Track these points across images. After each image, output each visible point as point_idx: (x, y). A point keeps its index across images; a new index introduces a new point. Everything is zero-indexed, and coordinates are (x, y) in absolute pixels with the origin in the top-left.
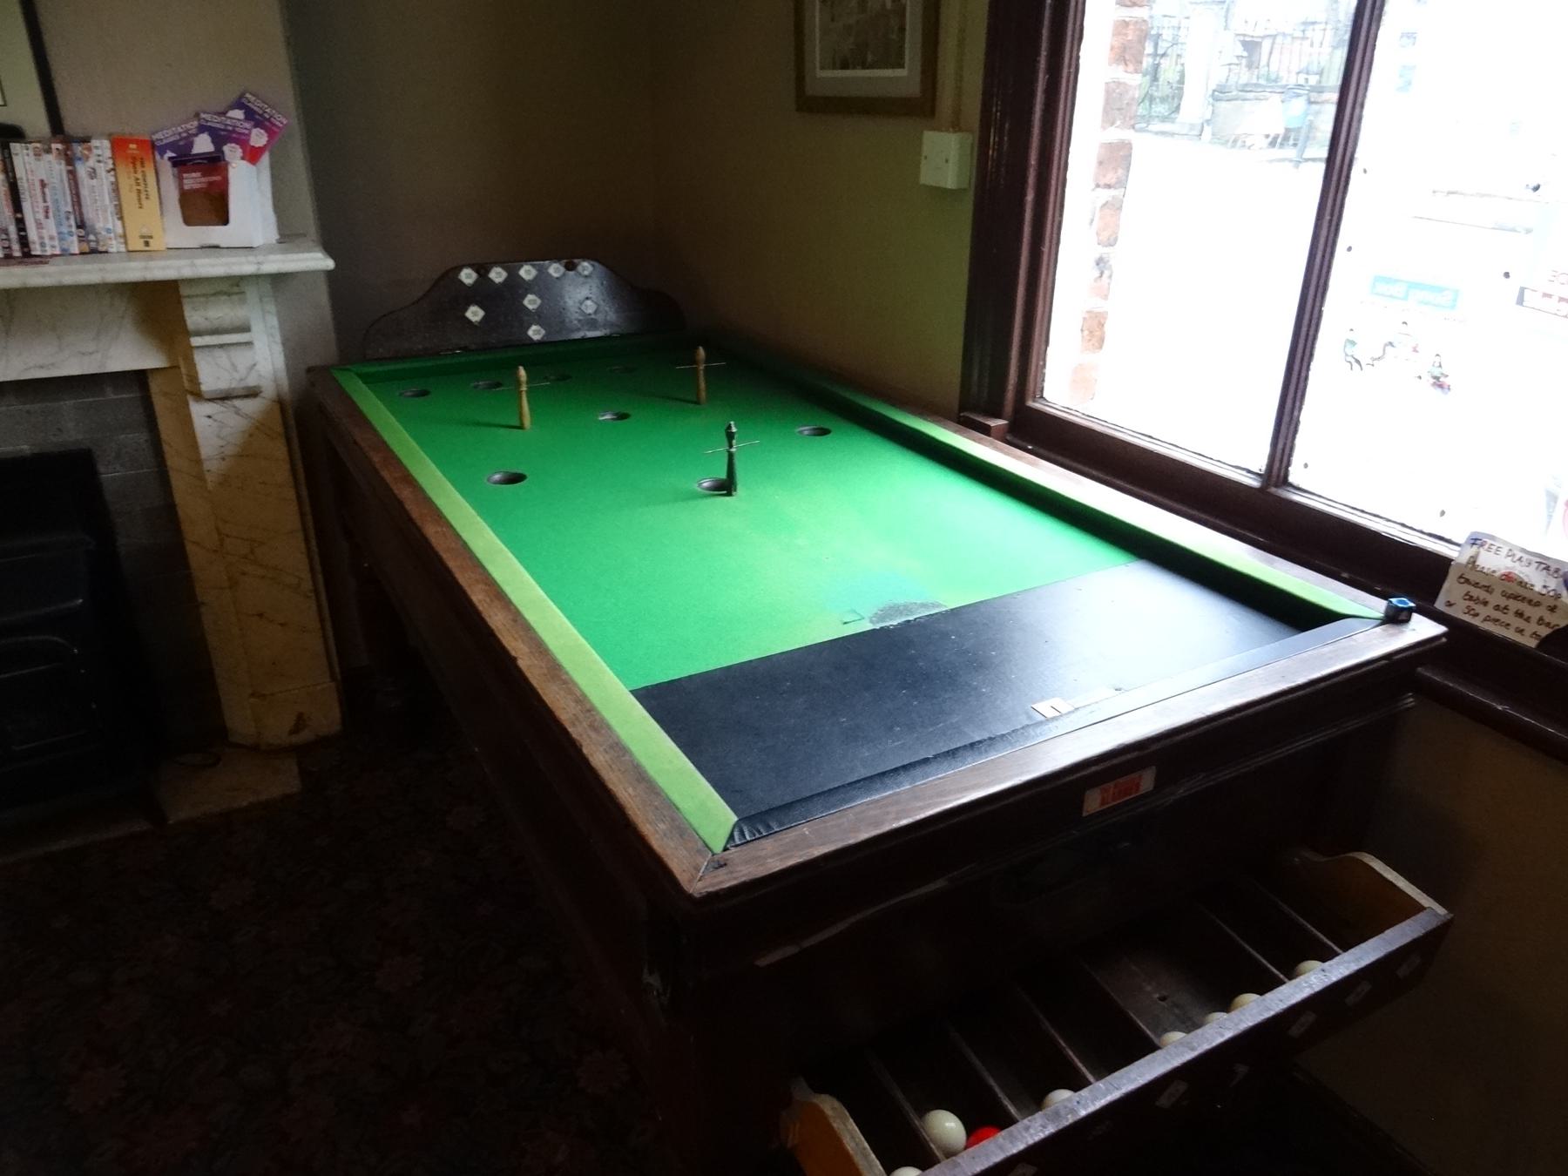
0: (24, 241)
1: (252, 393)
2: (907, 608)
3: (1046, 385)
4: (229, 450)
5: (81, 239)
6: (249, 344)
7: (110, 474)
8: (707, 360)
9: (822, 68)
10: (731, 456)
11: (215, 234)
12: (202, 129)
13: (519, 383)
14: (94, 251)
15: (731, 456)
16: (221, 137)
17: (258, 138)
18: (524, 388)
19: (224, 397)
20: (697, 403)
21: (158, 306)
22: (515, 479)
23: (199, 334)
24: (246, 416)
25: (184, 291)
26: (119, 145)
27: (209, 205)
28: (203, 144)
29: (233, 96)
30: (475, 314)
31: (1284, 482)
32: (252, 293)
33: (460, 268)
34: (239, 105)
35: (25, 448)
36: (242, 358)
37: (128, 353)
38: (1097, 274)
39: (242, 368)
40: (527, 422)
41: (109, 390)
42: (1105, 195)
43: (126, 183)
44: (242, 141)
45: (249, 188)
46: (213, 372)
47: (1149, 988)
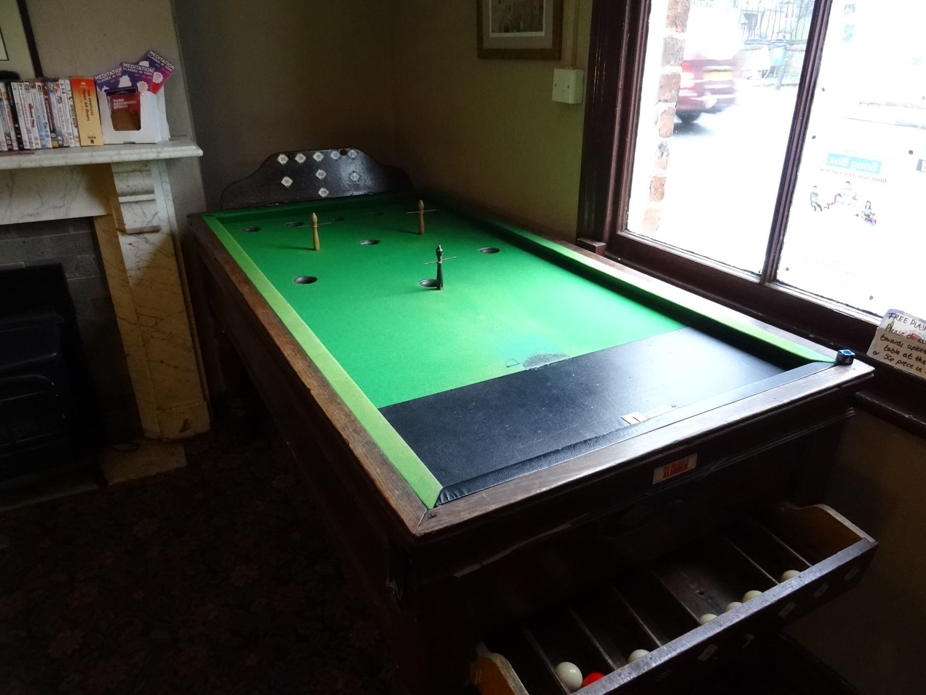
0: (20, 141)
1: (155, 230)
2: (544, 358)
3: (629, 221)
4: (143, 264)
6: (153, 200)
7: (72, 278)
8: (425, 209)
10: (439, 266)
11: (133, 135)
12: (124, 73)
13: (313, 224)
14: (61, 146)
15: (439, 266)
17: (158, 78)
19: (139, 233)
20: (420, 233)
22: (310, 280)
23: (124, 195)
25: (114, 169)
27: (129, 118)
28: (125, 82)
29: (142, 53)
31: (774, 279)
32: (155, 171)
33: (278, 155)
34: (146, 58)
35: (23, 264)
36: (149, 209)
37: (81, 206)
38: (659, 154)
39: (149, 217)
43: (79, 105)
44: (148, 80)
45: (152, 108)
46: (132, 218)
47: (693, 587)
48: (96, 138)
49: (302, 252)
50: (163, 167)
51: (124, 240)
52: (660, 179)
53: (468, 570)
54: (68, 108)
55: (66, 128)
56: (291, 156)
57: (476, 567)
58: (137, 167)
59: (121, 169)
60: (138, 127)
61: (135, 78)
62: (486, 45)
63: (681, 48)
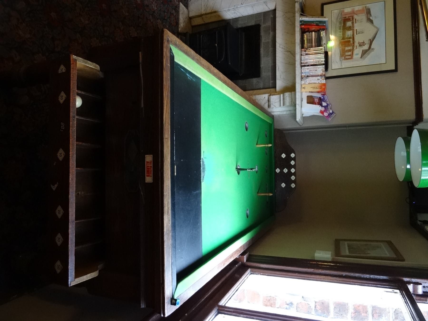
0: (305, 66)
1: (269, 106)
2: (204, 172)
3: (255, 275)
4: (257, 101)
5: (305, 76)
6: (280, 106)
7: (255, 80)
8: (269, 196)
9: (348, 244)
10: (246, 169)
11: (305, 101)
12: (328, 104)
13: (267, 144)
14: (302, 78)
15: (246, 169)
16: (326, 107)
17: (326, 114)
18: (266, 146)
19: (269, 101)
20: (258, 193)
21: (291, 89)
22: (247, 129)
23: (283, 96)
24: (264, 105)
25: (293, 93)
26: (324, 85)
27: (311, 100)
28: (324, 104)
29: (335, 112)
30: (284, 156)
31: (219, 312)
32: (291, 108)
33: (295, 154)
34: (333, 112)
35: (262, 66)
36: (277, 104)
37: (280, 84)
38: (288, 302)
39: (274, 104)
40: (258, 146)
41: (272, 82)
42: (313, 306)
43: (316, 85)
44: (325, 111)
45: (314, 110)
46: (274, 98)
47: (83, 193)
48: (305, 88)
49: (257, 139)
50: (293, 112)
51: (266, 96)
52: (275, 304)
53: (140, 56)
54: (315, 82)
55: (309, 80)
56: (294, 174)
57: (141, 61)
58: (293, 100)
59: (293, 95)
60: (308, 103)
61: (326, 107)
62: (341, 242)
63: (343, 316)
